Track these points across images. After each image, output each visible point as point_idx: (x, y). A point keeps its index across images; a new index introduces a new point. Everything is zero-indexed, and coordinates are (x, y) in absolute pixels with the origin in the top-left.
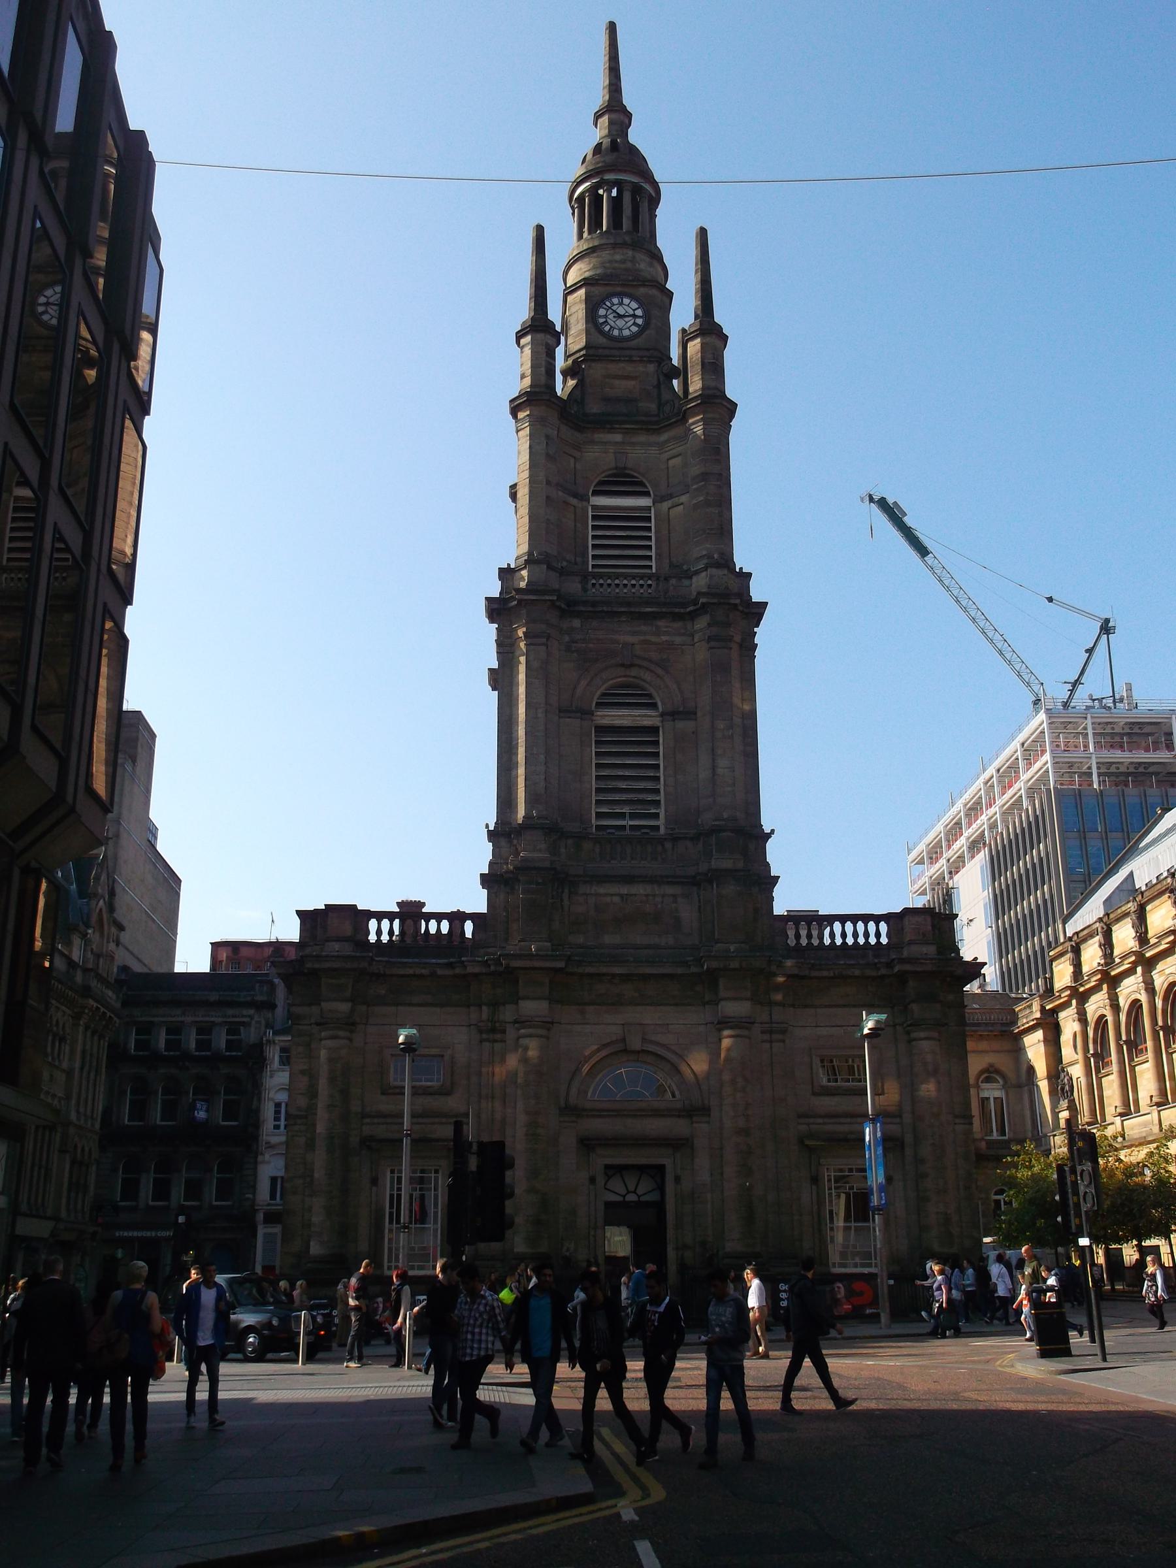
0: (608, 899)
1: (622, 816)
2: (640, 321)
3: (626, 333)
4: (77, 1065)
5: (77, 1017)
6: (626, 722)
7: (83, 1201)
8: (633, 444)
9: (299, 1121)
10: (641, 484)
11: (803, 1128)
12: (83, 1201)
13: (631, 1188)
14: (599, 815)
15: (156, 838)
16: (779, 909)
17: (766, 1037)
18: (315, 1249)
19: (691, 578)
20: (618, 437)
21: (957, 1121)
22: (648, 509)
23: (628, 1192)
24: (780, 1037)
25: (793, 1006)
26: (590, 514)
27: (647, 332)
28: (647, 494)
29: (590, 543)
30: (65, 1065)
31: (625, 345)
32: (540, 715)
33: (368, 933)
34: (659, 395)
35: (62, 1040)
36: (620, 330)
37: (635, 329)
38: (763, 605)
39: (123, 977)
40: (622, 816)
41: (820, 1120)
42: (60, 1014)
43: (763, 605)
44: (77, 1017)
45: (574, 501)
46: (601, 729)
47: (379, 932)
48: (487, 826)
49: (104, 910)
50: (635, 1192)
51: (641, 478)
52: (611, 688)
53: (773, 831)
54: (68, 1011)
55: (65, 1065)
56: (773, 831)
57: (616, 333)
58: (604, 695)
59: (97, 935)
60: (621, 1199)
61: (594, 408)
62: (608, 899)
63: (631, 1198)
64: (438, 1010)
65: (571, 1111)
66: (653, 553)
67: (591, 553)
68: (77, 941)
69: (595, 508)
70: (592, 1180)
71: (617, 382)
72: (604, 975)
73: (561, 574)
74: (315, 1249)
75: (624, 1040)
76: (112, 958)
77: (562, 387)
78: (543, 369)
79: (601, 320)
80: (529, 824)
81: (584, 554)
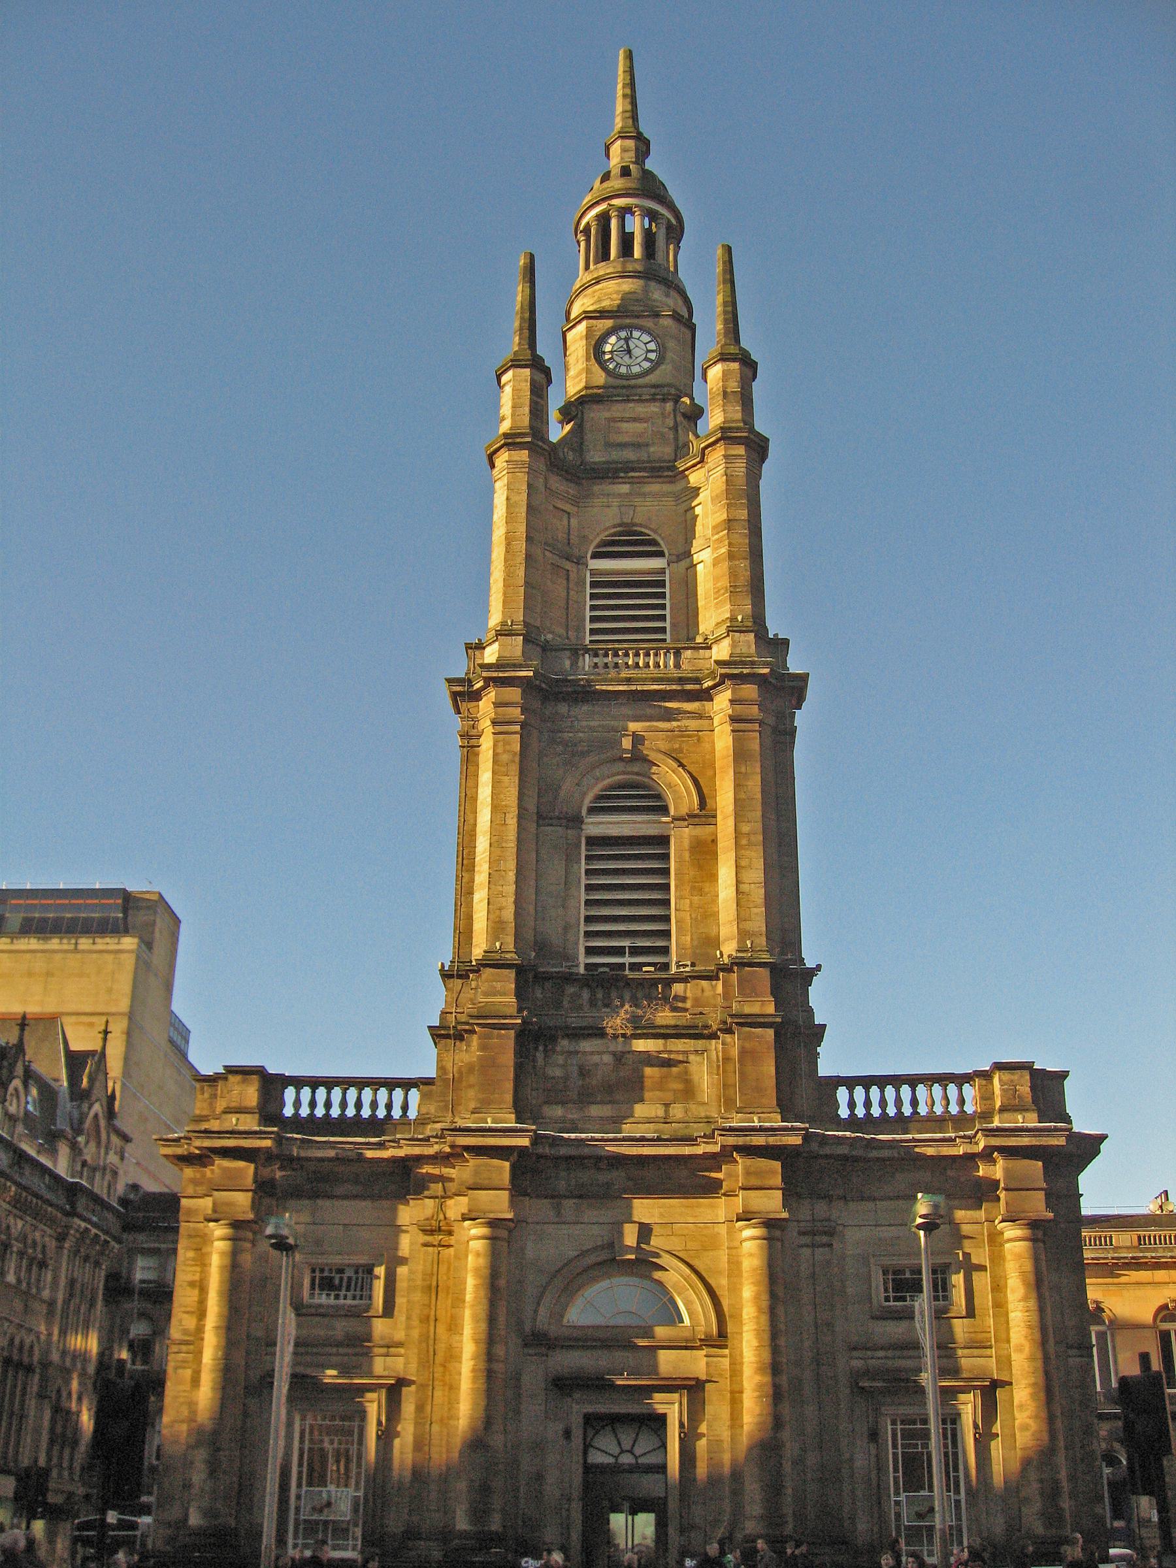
0: (596, 1058)
1: (619, 951)
2: (652, 356)
3: (636, 370)
4: (60, 1296)
5: (61, 1238)
6: (626, 831)
7: (71, 1459)
8: (644, 495)
9: (184, 1348)
10: (654, 542)
11: (857, 1364)
12: (71, 1459)
13: (627, 1445)
14: (590, 951)
15: (187, 1042)
16: (825, 1069)
17: (806, 1240)
18: (195, 1520)
19: (710, 648)
20: (625, 488)
21: (1070, 1352)
22: (662, 571)
23: (622, 1452)
24: (825, 1239)
25: (844, 1198)
26: (588, 580)
27: (663, 367)
28: (660, 554)
29: (588, 614)
30: (46, 1294)
31: (633, 382)
32: (509, 821)
33: (283, 1104)
34: (676, 439)
35: (43, 1265)
36: (629, 366)
37: (646, 365)
38: (804, 678)
39: (132, 1196)
40: (619, 951)
41: (881, 1354)
42: (37, 1234)
43: (804, 678)
44: (61, 1238)
45: (568, 565)
46: (592, 841)
47: (297, 1103)
48: (443, 965)
49: (101, 1115)
50: (631, 1452)
51: (654, 536)
52: (612, 787)
53: (819, 967)
54: (49, 1231)
55: (46, 1294)
56: (819, 967)
57: (623, 370)
58: (599, 798)
59: (92, 1145)
60: (611, 1460)
61: (596, 456)
62: (596, 1058)
63: (626, 1459)
64: (367, 1204)
65: (540, 1341)
66: (668, 625)
67: (588, 626)
68: (64, 1150)
69: (594, 573)
70: (567, 1434)
71: (625, 425)
72: (584, 1158)
73: (544, 650)
74: (195, 1520)
75: (611, 1245)
76: (115, 1173)
77: (557, 432)
78: (527, 410)
79: (607, 357)
80: (491, 962)
81: (580, 628)
